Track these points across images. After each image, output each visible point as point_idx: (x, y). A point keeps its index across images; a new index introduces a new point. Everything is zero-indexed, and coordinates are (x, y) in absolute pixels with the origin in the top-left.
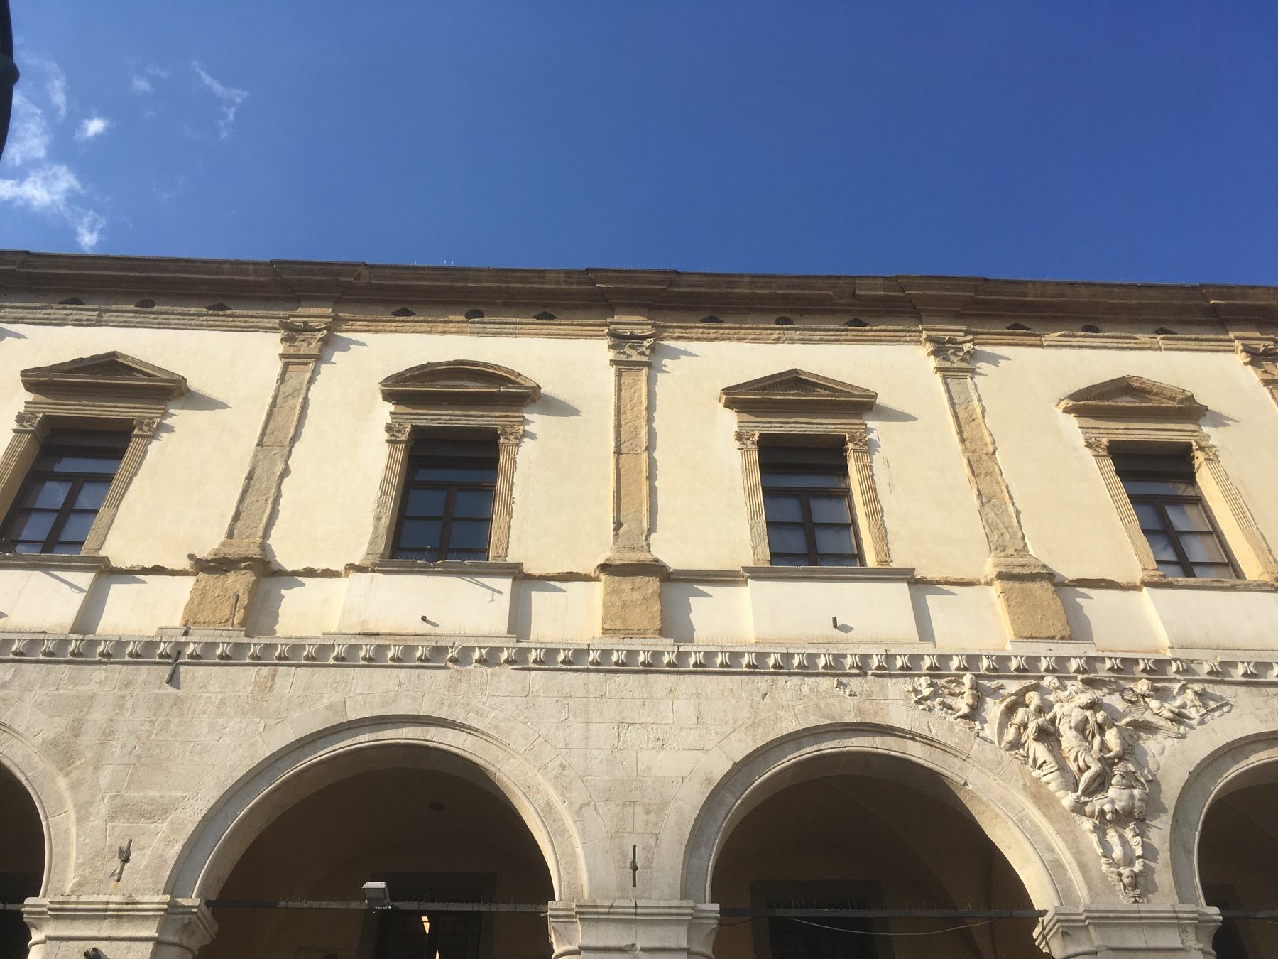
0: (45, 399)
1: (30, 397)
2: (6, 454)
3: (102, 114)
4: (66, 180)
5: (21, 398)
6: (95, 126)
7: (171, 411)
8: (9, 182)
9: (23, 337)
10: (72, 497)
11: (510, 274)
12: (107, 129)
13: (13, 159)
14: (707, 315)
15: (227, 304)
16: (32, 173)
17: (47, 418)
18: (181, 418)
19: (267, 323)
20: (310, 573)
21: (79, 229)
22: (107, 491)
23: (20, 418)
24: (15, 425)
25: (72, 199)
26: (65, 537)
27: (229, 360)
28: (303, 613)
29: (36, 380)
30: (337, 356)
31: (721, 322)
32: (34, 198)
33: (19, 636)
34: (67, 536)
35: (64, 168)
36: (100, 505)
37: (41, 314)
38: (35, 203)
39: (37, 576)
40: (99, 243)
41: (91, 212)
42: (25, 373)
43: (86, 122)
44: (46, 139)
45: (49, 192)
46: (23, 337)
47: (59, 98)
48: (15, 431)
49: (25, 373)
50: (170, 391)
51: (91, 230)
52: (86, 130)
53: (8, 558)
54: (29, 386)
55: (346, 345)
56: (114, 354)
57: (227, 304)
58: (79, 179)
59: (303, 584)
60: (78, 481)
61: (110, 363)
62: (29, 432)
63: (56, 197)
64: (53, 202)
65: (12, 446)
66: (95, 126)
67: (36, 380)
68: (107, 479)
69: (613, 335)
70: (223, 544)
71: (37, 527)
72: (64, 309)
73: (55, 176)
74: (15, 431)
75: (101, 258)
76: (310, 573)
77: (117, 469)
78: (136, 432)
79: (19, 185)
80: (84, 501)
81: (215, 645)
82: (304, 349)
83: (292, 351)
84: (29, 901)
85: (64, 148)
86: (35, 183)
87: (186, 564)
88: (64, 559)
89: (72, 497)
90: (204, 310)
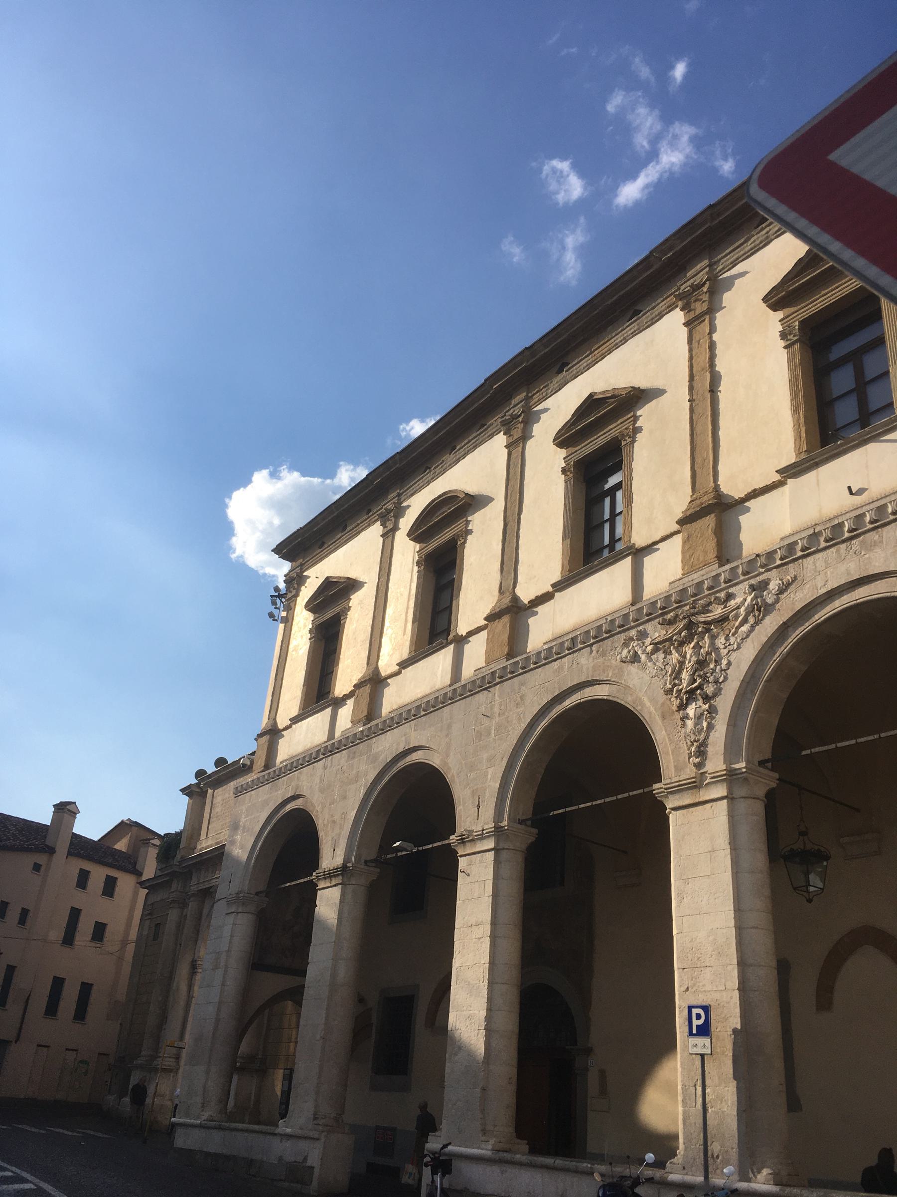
0: (792, 309)
1: (780, 315)
2: (790, 369)
3: (678, 59)
4: (685, 132)
5: (774, 320)
6: (680, 70)
7: (469, 518)
8: (650, 167)
9: (746, 273)
10: (859, 373)
11: (470, 399)
12: (689, 65)
13: (643, 147)
14: (556, 369)
15: (638, 308)
16: (659, 145)
17: (802, 323)
18: (646, 414)
19: (662, 306)
20: (756, 494)
21: (717, 163)
22: (886, 352)
23: (783, 335)
24: (782, 343)
25: (697, 142)
26: (873, 407)
27: (650, 355)
28: (765, 526)
29: (778, 299)
30: (728, 298)
31: (641, 311)
32: (673, 164)
33: (888, 499)
34: (874, 405)
35: (677, 124)
36: (888, 366)
37: (748, 246)
38: (676, 169)
39: (872, 447)
40: (738, 165)
41: (717, 142)
42: (765, 299)
43: (671, 73)
44: (656, 112)
45: (680, 152)
46: (746, 273)
47: (645, 72)
48: (785, 347)
49: (765, 299)
50: (632, 399)
51: (725, 159)
52: (675, 79)
53: (841, 445)
54: (775, 307)
55: (729, 284)
56: (591, 395)
57: (638, 308)
58: (692, 123)
59: (658, 549)
60: (856, 357)
61: (591, 403)
62: (796, 342)
63: (688, 150)
64: (687, 157)
65: (790, 361)
66: (680, 70)
67: (778, 299)
68: (880, 342)
69: (680, 297)
70: (499, 600)
71: (846, 411)
72: (763, 229)
73: (676, 137)
74: (785, 347)
75: (446, 415)
76: (756, 494)
77: (883, 329)
78: (623, 443)
79: (658, 163)
80: (871, 371)
81: (702, 582)
82: (699, 308)
83: (692, 315)
84: (655, 786)
85: (671, 108)
86: (667, 153)
87: (676, 527)
88: (886, 424)
89: (859, 373)
90: (366, 517)
